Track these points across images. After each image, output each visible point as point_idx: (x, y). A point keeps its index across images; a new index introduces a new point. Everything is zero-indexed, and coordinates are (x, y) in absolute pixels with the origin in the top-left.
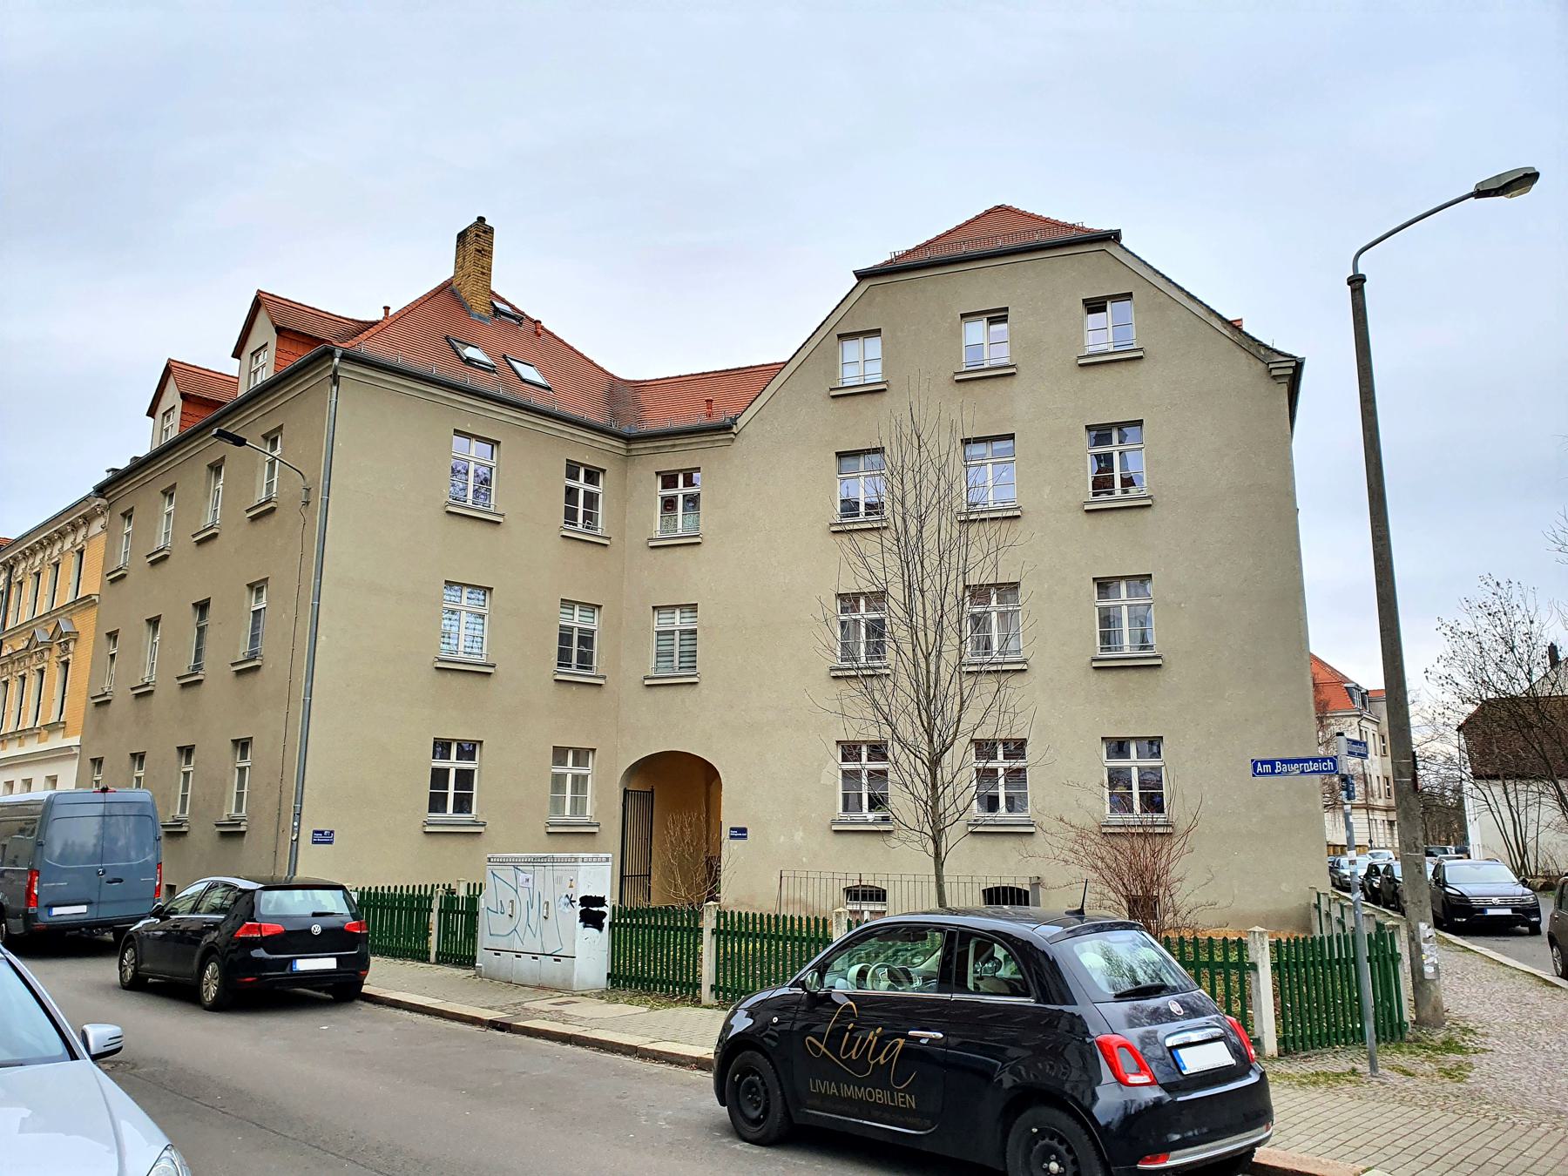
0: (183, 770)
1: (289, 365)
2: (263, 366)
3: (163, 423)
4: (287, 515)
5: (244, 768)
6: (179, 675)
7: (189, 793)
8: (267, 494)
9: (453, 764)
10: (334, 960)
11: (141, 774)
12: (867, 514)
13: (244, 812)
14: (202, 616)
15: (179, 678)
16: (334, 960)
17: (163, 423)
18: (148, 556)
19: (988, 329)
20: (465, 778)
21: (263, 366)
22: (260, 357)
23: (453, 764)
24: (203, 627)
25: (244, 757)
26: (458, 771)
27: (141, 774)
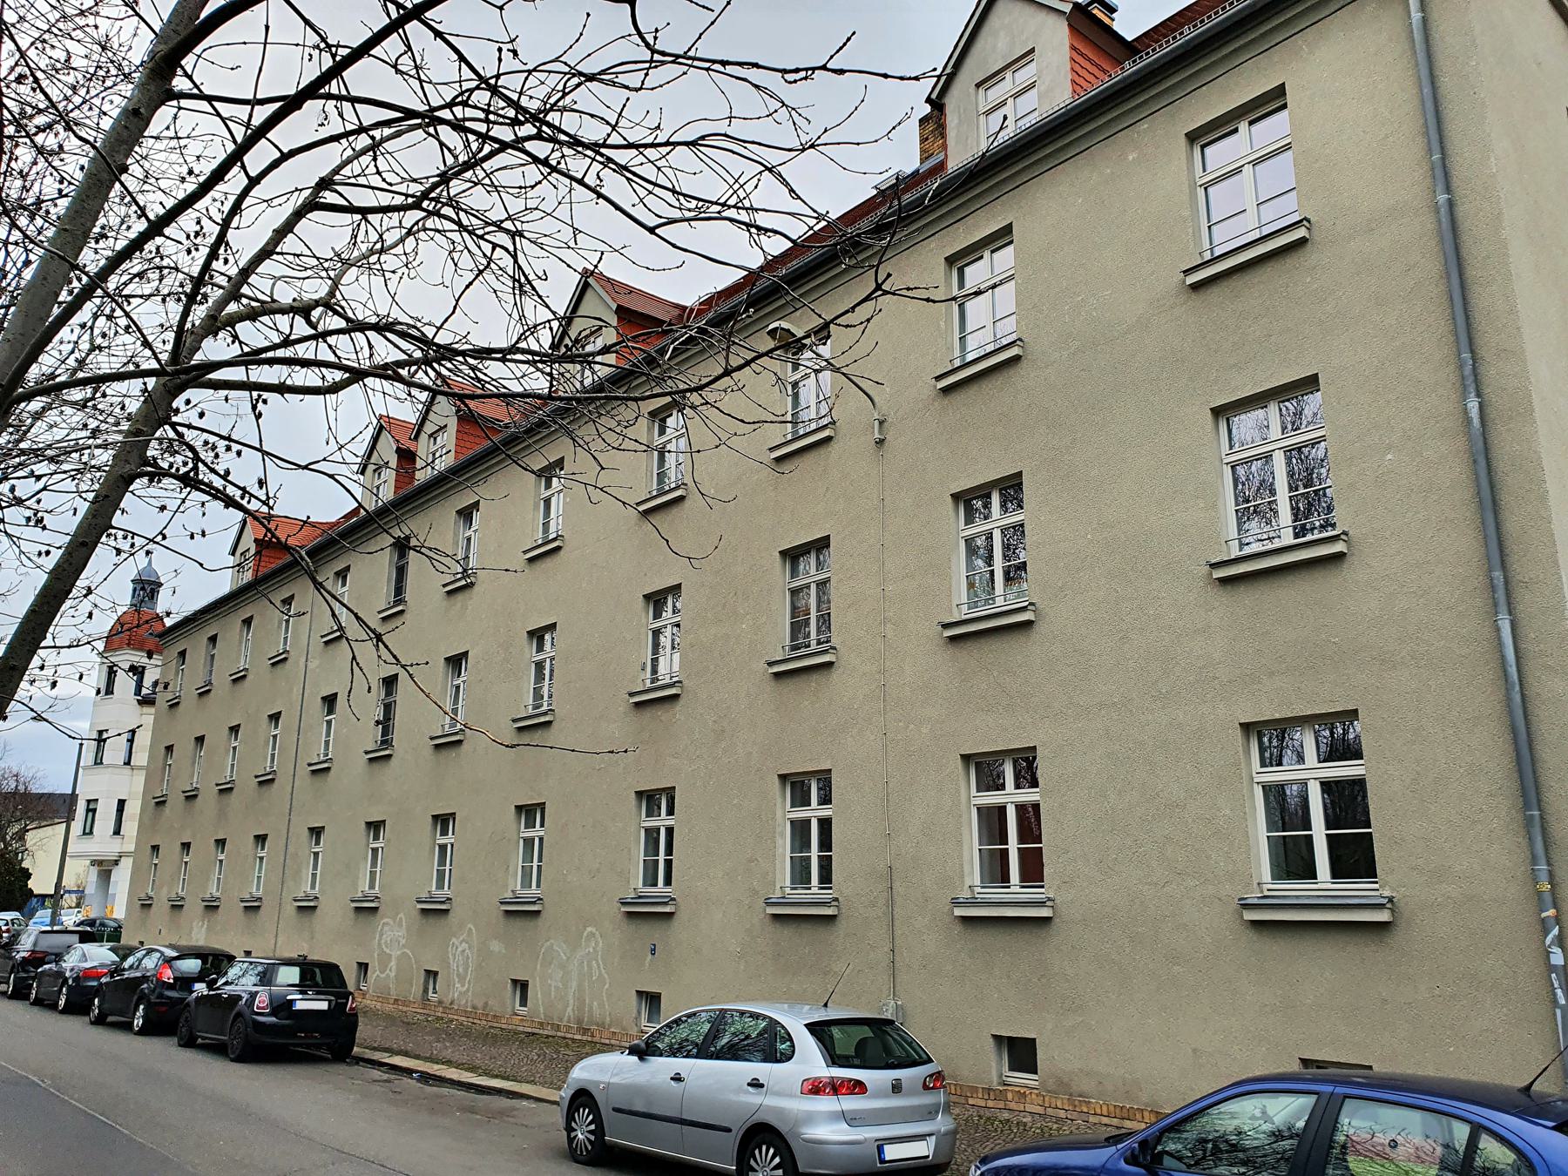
0: (371, 846)
1: (470, 453)
2: (385, 482)
3: (428, 447)
4: (850, 449)
5: (377, 849)
6: (947, 621)
7: (318, 872)
8: (658, 485)
9: (1011, 796)
10: (327, 1003)
11: (222, 857)
12: (819, 643)
13: (377, 888)
14: (389, 693)
15: (514, 721)
16: (327, 1003)
17: (428, 447)
18: (231, 675)
19: (108, 766)
20: (1030, 817)
21: (385, 482)
22: (439, 439)
23: (1011, 796)
24: (390, 704)
25: (376, 838)
26: (1327, 786)
27: (222, 857)
